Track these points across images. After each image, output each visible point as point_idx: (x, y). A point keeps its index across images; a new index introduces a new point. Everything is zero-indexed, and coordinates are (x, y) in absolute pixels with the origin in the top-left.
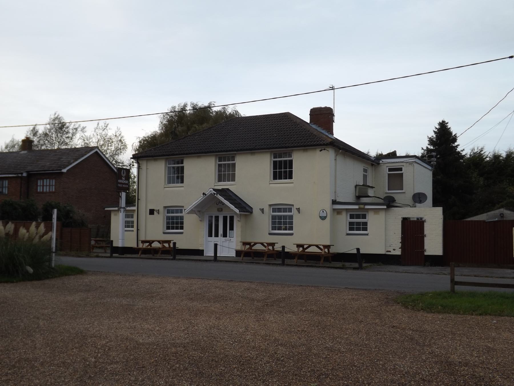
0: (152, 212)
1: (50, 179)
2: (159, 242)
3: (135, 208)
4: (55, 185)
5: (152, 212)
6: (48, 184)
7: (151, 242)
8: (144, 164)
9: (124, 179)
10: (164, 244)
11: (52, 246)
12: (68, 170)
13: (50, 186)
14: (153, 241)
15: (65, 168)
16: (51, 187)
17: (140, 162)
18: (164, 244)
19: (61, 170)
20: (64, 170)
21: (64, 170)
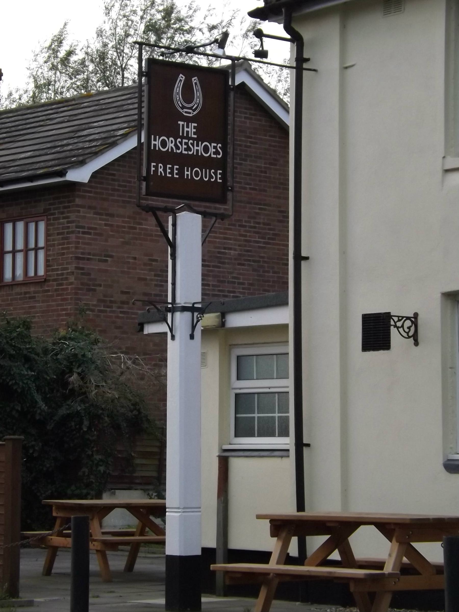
0: (377, 332)
1: (27, 217)
2: (387, 527)
3: (283, 316)
4: (47, 248)
5: (377, 332)
6: (20, 245)
7: (340, 530)
8: (325, 38)
9: (191, 129)
10: (422, 547)
11: (112, 490)
12: (95, 175)
13: (26, 250)
14: (351, 525)
15: (82, 163)
16: (32, 255)
17: (307, 34)
18: (422, 547)
19: (62, 173)
20: (81, 175)
21: (81, 175)
